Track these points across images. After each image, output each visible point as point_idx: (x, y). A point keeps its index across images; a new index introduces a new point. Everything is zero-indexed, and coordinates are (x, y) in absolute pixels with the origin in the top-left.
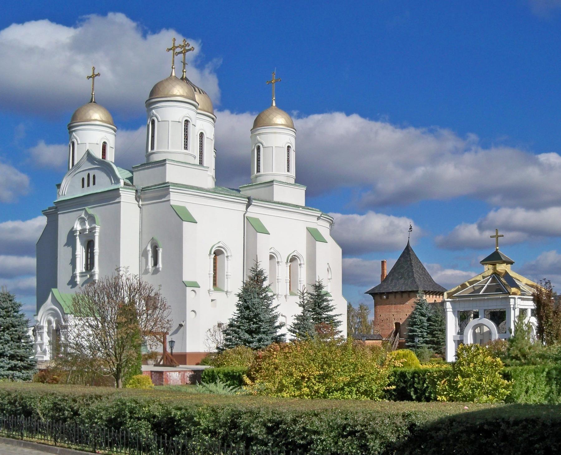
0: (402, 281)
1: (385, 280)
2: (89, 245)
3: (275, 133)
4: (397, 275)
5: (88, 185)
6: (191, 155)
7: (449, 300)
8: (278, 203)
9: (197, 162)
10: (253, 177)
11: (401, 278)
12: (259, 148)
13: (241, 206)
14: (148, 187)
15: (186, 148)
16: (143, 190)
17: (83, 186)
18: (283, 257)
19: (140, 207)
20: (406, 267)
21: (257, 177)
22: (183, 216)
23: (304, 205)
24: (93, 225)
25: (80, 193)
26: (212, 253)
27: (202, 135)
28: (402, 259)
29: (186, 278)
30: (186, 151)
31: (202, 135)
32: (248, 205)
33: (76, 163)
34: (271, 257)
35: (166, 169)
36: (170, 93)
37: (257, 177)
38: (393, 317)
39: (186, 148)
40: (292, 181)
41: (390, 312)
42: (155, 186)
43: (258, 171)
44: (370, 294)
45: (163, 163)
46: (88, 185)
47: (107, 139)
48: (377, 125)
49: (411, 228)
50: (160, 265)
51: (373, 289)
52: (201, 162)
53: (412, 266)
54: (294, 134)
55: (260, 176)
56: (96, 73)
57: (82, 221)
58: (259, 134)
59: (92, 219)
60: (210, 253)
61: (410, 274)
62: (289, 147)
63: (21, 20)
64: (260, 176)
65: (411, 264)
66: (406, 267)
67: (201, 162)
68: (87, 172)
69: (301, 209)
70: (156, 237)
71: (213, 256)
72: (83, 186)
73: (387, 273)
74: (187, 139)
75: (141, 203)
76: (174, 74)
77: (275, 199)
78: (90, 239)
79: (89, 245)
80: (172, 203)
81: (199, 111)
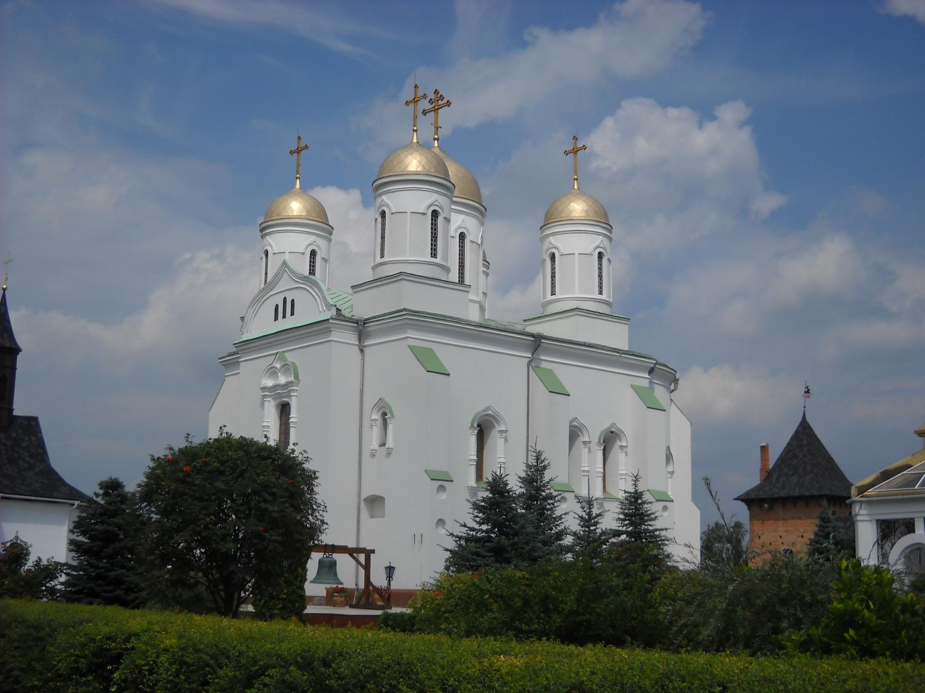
0: (795, 479)
1: (768, 476)
2: (284, 409)
4: (786, 470)
5: (284, 317)
9: (454, 276)
11: (793, 475)
12: (553, 257)
13: (355, 541)
14: (375, 317)
15: (434, 255)
17: (276, 318)
18: (593, 434)
19: (362, 351)
20: (800, 456)
27: (462, 236)
28: (2, 311)
30: (433, 260)
31: (462, 236)
38: (781, 541)
42: (385, 315)
43: (553, 293)
44: (742, 500)
46: (284, 317)
47: (320, 248)
48: (94, 607)
49: (808, 392)
51: (748, 493)
56: (303, 145)
58: (553, 234)
59: (287, 368)
60: (472, 426)
63: (324, 185)
66: (800, 456)
72: (276, 318)
73: (771, 464)
76: (415, 140)
79: (284, 409)
81: (454, 199)
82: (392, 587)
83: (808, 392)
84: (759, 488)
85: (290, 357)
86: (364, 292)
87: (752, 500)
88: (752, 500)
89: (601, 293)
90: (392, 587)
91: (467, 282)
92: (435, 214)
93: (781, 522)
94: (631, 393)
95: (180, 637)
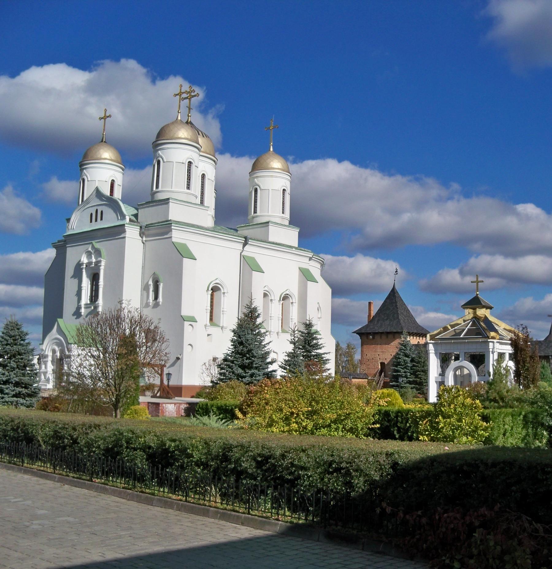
0: (387, 322)
1: (371, 321)
2: (95, 278)
3: (272, 176)
5: (96, 220)
6: (193, 195)
7: (432, 342)
8: (273, 243)
9: (198, 201)
10: (250, 217)
11: (387, 319)
14: (152, 224)
15: (188, 188)
16: (147, 226)
17: (91, 221)
18: (276, 295)
19: (143, 243)
21: (253, 217)
22: (183, 252)
23: (297, 246)
24: (99, 259)
25: (88, 227)
26: (210, 289)
27: (203, 176)
28: (388, 301)
29: (185, 312)
30: (188, 191)
31: (203, 176)
32: (245, 244)
33: (85, 199)
34: (265, 295)
35: (169, 207)
36: (176, 136)
37: (253, 217)
39: (188, 188)
40: (287, 223)
41: (375, 351)
42: (159, 223)
43: (255, 212)
44: (357, 333)
45: (166, 201)
46: (96, 220)
47: (116, 178)
49: (396, 271)
50: (160, 299)
52: (202, 202)
53: (397, 308)
54: (289, 178)
55: (257, 217)
56: (107, 115)
57: (89, 254)
58: (257, 177)
59: (98, 253)
60: (208, 289)
61: (396, 315)
62: (284, 190)
64: (257, 217)
65: (396, 305)
67: (202, 202)
68: (95, 208)
69: (294, 249)
70: (157, 273)
71: (210, 292)
72: (91, 221)
73: (373, 313)
74: (189, 180)
75: (144, 239)
76: (179, 118)
77: (271, 239)
78: (95, 272)
79: (95, 278)
80: (174, 240)
81: (201, 154)
82: (171, 383)
83: (396, 271)
84: (367, 326)
85: (97, 245)
86: (150, 208)
87: (363, 334)
88: (363, 334)
89: (283, 213)
90: (170, 384)
91: (206, 203)
92: (190, 163)
93: (379, 346)
94: (297, 272)
95: (253, 417)
